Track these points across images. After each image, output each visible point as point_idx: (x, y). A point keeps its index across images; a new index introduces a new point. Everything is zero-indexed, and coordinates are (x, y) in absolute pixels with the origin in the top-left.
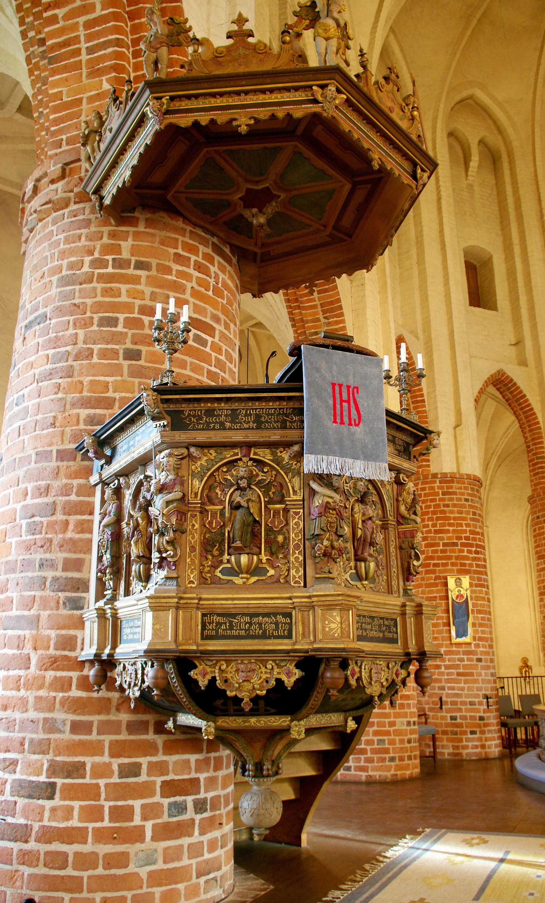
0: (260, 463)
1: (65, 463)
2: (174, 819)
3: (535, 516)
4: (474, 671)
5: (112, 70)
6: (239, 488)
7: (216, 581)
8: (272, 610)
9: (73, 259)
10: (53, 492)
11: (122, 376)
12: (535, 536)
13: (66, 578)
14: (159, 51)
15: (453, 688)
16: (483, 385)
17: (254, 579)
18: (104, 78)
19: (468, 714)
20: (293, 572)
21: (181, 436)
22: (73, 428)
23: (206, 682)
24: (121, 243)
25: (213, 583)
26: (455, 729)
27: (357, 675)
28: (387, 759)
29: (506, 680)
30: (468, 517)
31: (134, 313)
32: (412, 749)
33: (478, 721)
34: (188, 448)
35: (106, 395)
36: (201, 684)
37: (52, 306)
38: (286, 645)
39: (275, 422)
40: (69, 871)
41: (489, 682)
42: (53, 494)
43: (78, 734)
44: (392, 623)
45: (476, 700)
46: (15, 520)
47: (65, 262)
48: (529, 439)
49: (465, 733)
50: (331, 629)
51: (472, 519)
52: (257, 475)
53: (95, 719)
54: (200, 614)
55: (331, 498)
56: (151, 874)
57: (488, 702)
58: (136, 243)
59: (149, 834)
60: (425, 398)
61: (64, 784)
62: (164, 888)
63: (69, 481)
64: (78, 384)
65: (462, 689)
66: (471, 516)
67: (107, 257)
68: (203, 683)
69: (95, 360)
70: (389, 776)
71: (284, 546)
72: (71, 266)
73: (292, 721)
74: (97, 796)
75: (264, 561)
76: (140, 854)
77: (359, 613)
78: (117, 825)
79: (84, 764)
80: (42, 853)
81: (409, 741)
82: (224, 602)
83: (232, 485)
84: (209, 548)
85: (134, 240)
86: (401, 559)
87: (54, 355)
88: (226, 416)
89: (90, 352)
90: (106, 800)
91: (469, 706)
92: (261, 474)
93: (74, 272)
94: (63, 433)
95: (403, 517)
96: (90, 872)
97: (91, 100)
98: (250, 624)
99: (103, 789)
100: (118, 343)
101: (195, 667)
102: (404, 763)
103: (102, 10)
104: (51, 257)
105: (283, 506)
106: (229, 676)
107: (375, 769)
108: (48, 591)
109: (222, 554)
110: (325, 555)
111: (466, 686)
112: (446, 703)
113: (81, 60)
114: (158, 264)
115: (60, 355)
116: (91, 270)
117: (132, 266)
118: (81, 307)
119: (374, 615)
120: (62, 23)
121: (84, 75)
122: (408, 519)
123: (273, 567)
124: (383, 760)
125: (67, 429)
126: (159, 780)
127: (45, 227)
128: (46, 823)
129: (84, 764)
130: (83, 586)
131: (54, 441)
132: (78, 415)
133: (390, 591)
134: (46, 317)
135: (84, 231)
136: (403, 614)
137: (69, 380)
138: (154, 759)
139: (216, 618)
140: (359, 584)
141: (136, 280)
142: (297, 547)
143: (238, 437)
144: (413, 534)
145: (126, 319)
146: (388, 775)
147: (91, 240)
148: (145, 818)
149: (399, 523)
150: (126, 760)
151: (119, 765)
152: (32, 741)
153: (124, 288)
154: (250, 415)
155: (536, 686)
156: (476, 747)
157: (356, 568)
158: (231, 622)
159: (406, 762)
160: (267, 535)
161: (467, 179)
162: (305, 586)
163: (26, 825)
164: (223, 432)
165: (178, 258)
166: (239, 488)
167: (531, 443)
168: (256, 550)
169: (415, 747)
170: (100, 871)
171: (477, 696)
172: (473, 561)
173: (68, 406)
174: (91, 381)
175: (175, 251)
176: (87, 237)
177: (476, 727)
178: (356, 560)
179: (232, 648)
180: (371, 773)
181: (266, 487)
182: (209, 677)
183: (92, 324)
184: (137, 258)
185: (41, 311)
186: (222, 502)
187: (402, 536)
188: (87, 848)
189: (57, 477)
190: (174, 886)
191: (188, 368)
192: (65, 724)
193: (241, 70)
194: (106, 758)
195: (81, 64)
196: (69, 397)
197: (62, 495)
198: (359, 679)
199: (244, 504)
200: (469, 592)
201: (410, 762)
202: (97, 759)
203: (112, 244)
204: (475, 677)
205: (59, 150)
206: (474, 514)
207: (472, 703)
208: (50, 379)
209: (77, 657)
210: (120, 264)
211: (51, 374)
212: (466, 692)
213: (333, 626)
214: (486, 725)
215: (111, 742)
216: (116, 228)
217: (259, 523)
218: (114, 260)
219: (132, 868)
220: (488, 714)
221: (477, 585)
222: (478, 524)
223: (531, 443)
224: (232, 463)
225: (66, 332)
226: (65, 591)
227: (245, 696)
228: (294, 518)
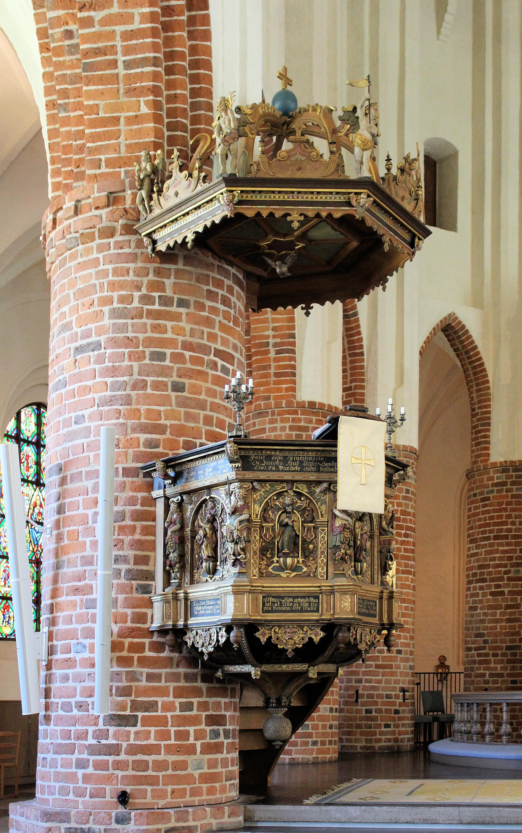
0: (299, 495)
1: (130, 479)
2: (213, 741)
3: (472, 493)
4: (393, 663)
5: (150, 92)
6: (285, 512)
7: (269, 575)
8: (307, 595)
9: (123, 293)
10: (121, 502)
11: (171, 406)
12: (469, 517)
13: (137, 570)
14: (383, 426)
15: (370, 681)
16: (431, 333)
17: (294, 574)
18: (141, 99)
19: (384, 708)
20: (320, 569)
21: (249, 475)
22: (135, 450)
23: (265, 640)
24: (165, 280)
25: (267, 576)
26: (369, 723)
27: (355, 636)
28: (310, 743)
29: (422, 675)
30: (401, 495)
31: (177, 349)
32: (333, 735)
33: (393, 715)
34: (252, 483)
35: (159, 422)
36: (262, 640)
37: (107, 336)
38: (316, 616)
39: (313, 467)
40: (150, 772)
41: (406, 675)
42: (122, 504)
43: (151, 682)
44: (374, 604)
45: (393, 693)
46: (88, 523)
47: (115, 295)
48: (476, 400)
49: (379, 726)
50: (345, 607)
51: (405, 498)
52: (297, 502)
53: (163, 671)
54: (261, 597)
55: (347, 521)
56: (201, 775)
57: (404, 695)
58: (177, 281)
59: (199, 749)
60: (365, 350)
61: (143, 716)
62: (208, 785)
63: (135, 494)
64: (137, 412)
65: (380, 682)
66: (404, 494)
67: (153, 294)
68: (263, 640)
69: (149, 391)
70: (311, 759)
71: (313, 552)
72: (122, 299)
73: (309, 667)
74: (166, 724)
75: (301, 562)
76: (194, 762)
77: (360, 597)
78: (179, 742)
79: (157, 702)
80: (130, 761)
81: (331, 727)
82: (277, 589)
83: (280, 509)
84: (265, 553)
85: (175, 278)
86: (381, 560)
87: (113, 383)
88: (280, 461)
89: (144, 383)
90: (171, 726)
91: (385, 700)
92: (299, 501)
93: (125, 306)
94: (126, 453)
95: (384, 530)
96: (164, 773)
97: (130, 121)
98: (293, 603)
99: (169, 719)
100: (166, 376)
101: (258, 630)
102: (326, 747)
103: (141, 23)
104: (100, 286)
105: (313, 525)
106: (280, 636)
107: (297, 752)
108: (123, 580)
109: (273, 557)
110: (342, 559)
111: (384, 678)
112: (363, 696)
113: (117, 74)
114: (195, 301)
115: (118, 385)
116: (141, 306)
117: (175, 304)
118: (134, 341)
119: (365, 598)
120: (97, 28)
121: (122, 91)
122: (387, 531)
123: (306, 566)
124: (306, 744)
125: (130, 450)
126: (204, 714)
127: (88, 251)
128: (132, 742)
129: (157, 702)
130: (150, 576)
131: (120, 459)
132: (138, 439)
133: (372, 582)
134: (101, 346)
135: (132, 265)
136: (381, 598)
137: (128, 407)
138: (201, 700)
139: (272, 600)
140: (355, 577)
141: (177, 317)
142: (322, 553)
143: (288, 476)
144: (389, 543)
145: (172, 354)
146: (310, 757)
147: (138, 275)
148: (196, 739)
149: (381, 534)
150: (184, 700)
151: (180, 703)
152: (117, 688)
153: (169, 324)
154: (296, 461)
155: (449, 689)
156: (389, 740)
157: (355, 566)
158: (281, 602)
159: (327, 746)
160: (302, 544)
161: (438, 38)
162: (327, 579)
163: (118, 744)
164: (278, 473)
165: (211, 296)
166: (285, 512)
167: (476, 406)
168: (296, 554)
169: (336, 732)
170: (170, 772)
171: (394, 689)
172: (401, 545)
173: (129, 431)
174: (147, 409)
175: (208, 287)
176: (134, 272)
177: (390, 721)
178: (355, 561)
179: (282, 618)
180: (294, 756)
181: (303, 511)
182: (267, 636)
183: (145, 358)
184: (178, 296)
185: (93, 339)
186: (273, 521)
187: (382, 543)
188: (161, 757)
189: (124, 490)
190: (214, 784)
191: (218, 397)
192: (142, 676)
193: (298, 175)
194: (171, 699)
195: (118, 77)
196: (130, 422)
197: (130, 505)
198: (355, 639)
199: (290, 523)
200: (394, 579)
201: (330, 747)
202: (165, 699)
203: (158, 281)
204: (394, 670)
205: (98, 172)
206: (407, 491)
207: (388, 696)
208: (111, 405)
209: (149, 628)
210: (165, 301)
211: (111, 400)
212: (383, 684)
213: (346, 604)
214: (400, 719)
215: (174, 688)
216: (160, 265)
217: (298, 536)
218: (160, 297)
219: (189, 771)
220: (404, 708)
221: (403, 572)
222: (410, 503)
223: (476, 406)
224: (280, 495)
225: (122, 363)
226: (137, 580)
227: (290, 647)
228: (321, 534)
